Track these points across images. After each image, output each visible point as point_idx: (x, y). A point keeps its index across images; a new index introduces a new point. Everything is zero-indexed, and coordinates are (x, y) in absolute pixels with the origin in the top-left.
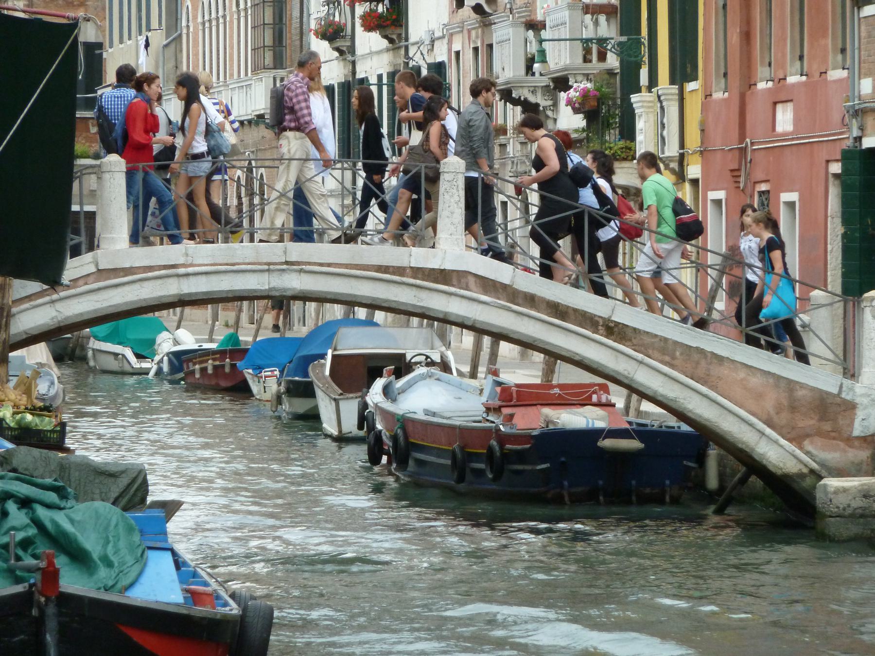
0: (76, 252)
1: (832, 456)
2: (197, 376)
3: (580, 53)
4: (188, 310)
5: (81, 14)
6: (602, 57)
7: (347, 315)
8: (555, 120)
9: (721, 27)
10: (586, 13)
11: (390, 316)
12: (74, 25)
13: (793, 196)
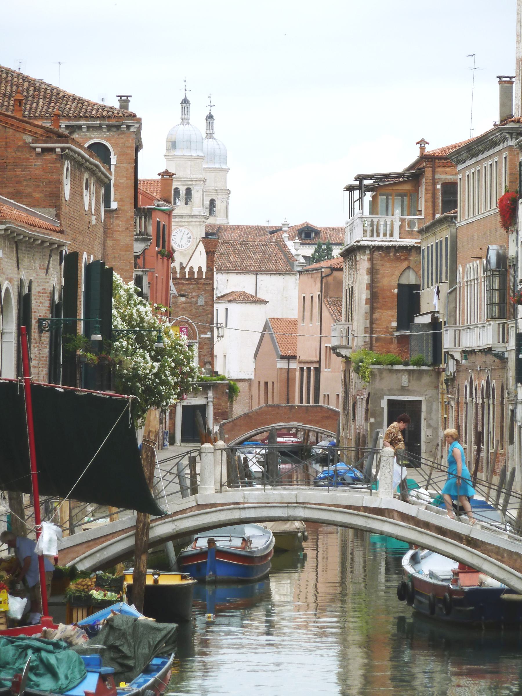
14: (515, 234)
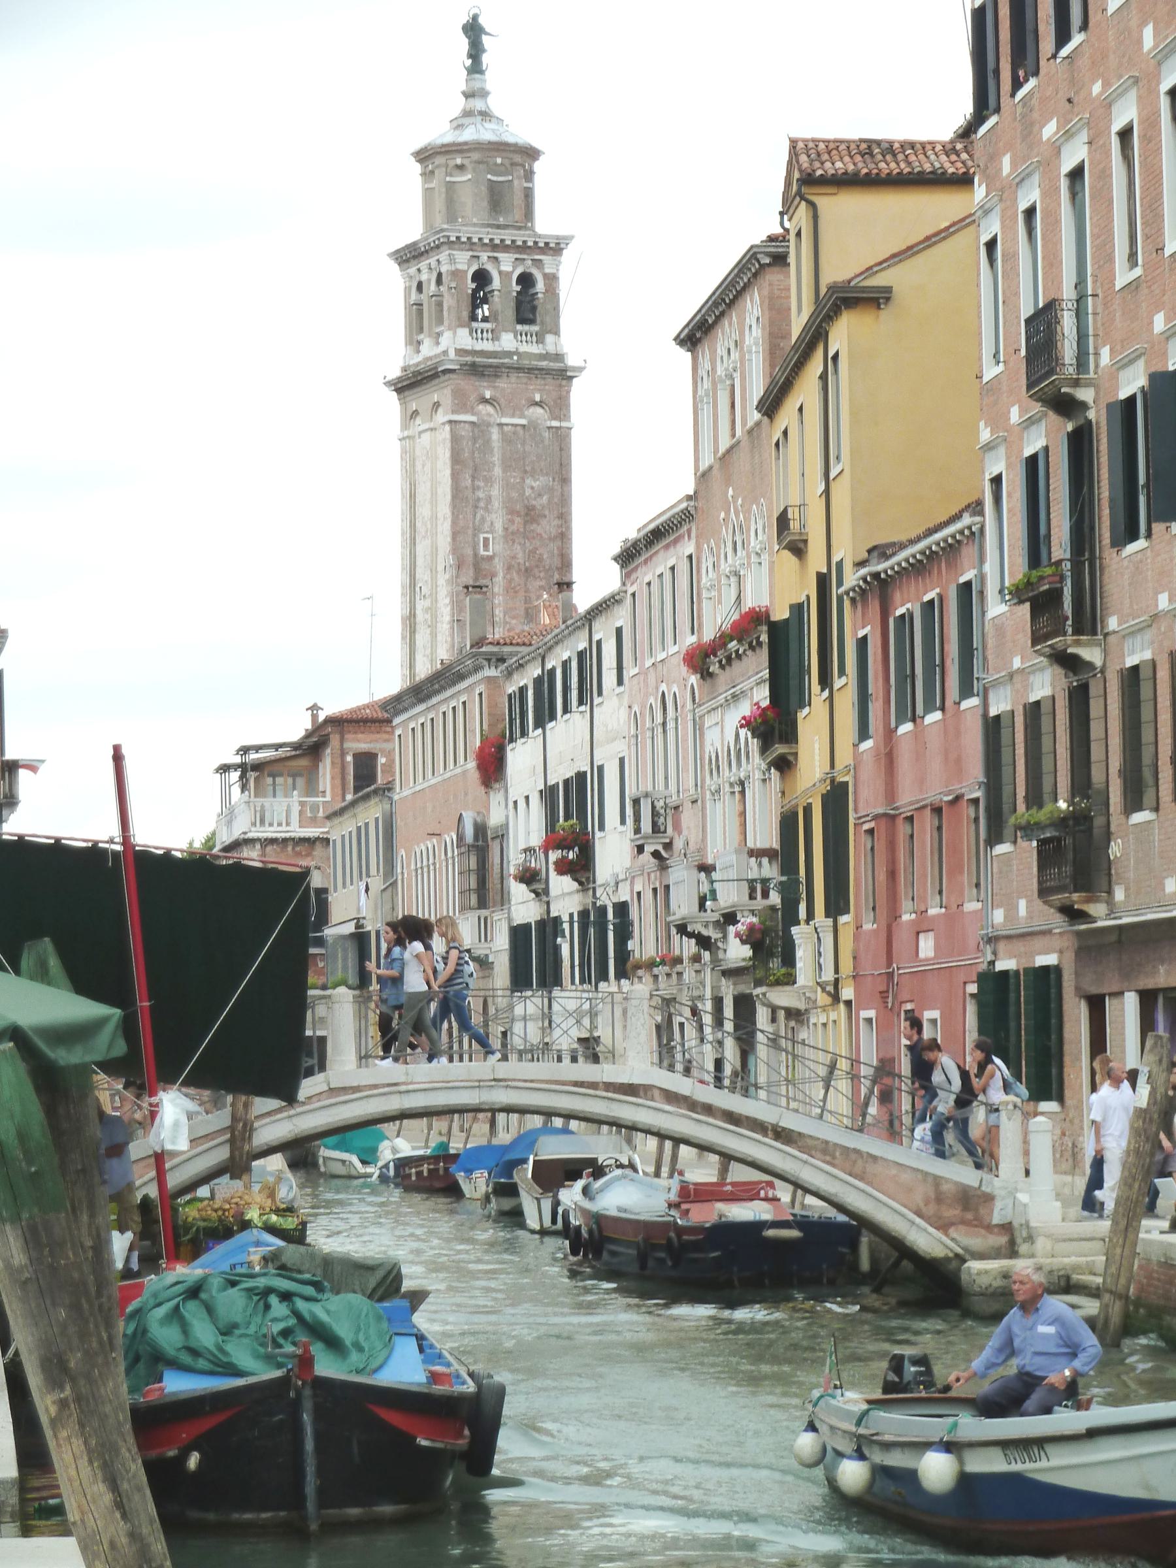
0: (309, 1073)
1: (976, 1241)
2: (414, 1178)
3: (746, 892)
4: (405, 1121)
5: (313, 864)
6: (765, 895)
7: (545, 1124)
8: (725, 951)
9: (870, 867)
10: (751, 856)
11: (583, 1124)
12: (305, 874)
13: (935, 1014)
14: (502, 791)
